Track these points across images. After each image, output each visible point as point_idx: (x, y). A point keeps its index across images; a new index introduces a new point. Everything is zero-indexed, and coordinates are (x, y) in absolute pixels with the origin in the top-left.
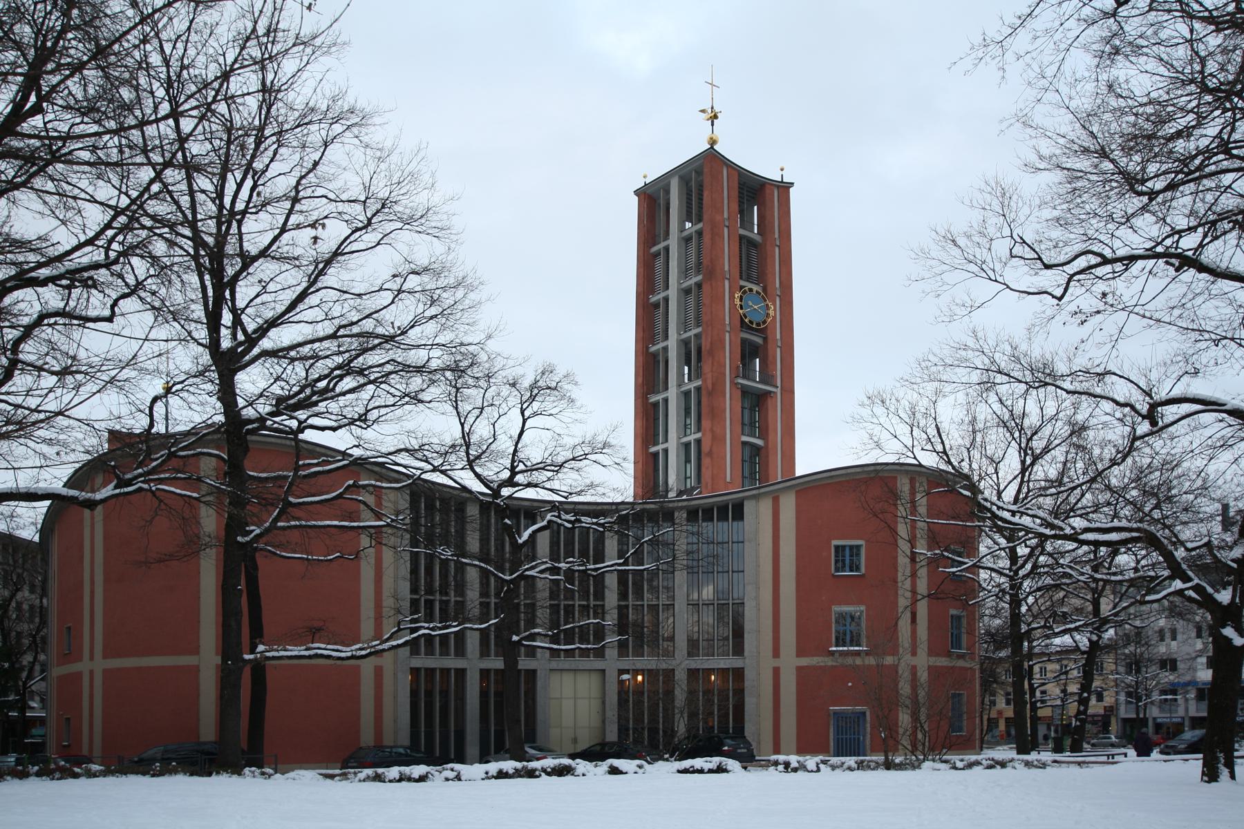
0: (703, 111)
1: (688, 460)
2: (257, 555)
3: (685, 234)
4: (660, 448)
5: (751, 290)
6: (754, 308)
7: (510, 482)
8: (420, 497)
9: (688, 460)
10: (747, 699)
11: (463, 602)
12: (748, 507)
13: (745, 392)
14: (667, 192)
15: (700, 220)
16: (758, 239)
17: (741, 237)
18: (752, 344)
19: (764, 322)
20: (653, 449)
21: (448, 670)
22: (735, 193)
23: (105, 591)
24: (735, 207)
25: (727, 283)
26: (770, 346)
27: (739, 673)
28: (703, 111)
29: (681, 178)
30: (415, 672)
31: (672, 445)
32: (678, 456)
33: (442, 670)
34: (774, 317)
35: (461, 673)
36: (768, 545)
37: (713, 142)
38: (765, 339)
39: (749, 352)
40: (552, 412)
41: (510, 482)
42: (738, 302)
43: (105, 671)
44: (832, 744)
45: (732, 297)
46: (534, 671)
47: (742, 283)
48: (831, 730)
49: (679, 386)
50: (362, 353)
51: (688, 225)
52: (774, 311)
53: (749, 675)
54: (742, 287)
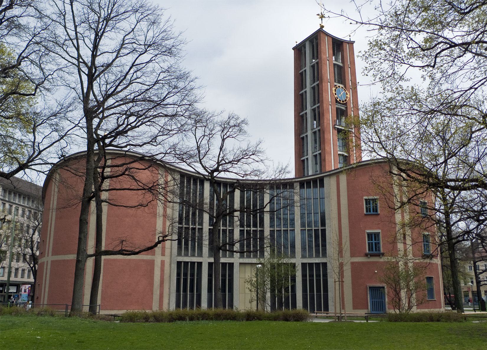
0: (318, 15)
1: (316, 164)
2: (103, 204)
3: (313, 64)
4: (305, 158)
5: (339, 87)
6: (341, 95)
7: (217, 170)
8: (197, 180)
9: (316, 164)
10: (329, 279)
11: (202, 229)
12: (326, 180)
13: (339, 131)
14: (305, 48)
15: (318, 58)
16: (341, 64)
17: (334, 64)
18: (341, 110)
19: (346, 100)
20: (302, 159)
21: (194, 263)
22: (331, 46)
23: (55, 223)
24: (331, 52)
25: (329, 84)
26: (348, 110)
27: (325, 265)
28: (318, 15)
29: (310, 41)
30: (179, 263)
31: (310, 156)
32: (312, 161)
33: (191, 262)
34: (350, 98)
35: (200, 264)
36: (335, 198)
37: (322, 27)
38: (346, 108)
39: (341, 113)
40: (234, 136)
41: (217, 170)
42: (334, 92)
43: (52, 261)
44: (369, 304)
45: (331, 90)
46: (233, 263)
47: (335, 84)
48: (369, 296)
49: (312, 130)
50: (148, 107)
51: (314, 60)
52: (349, 95)
53: (329, 266)
54: (335, 86)
